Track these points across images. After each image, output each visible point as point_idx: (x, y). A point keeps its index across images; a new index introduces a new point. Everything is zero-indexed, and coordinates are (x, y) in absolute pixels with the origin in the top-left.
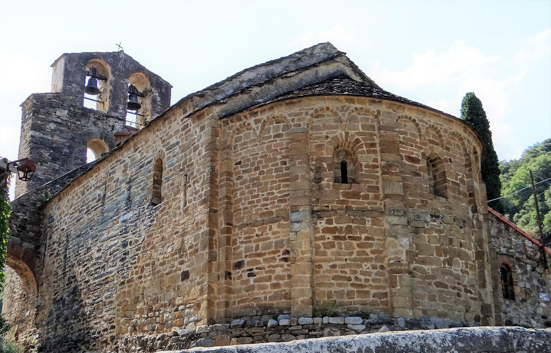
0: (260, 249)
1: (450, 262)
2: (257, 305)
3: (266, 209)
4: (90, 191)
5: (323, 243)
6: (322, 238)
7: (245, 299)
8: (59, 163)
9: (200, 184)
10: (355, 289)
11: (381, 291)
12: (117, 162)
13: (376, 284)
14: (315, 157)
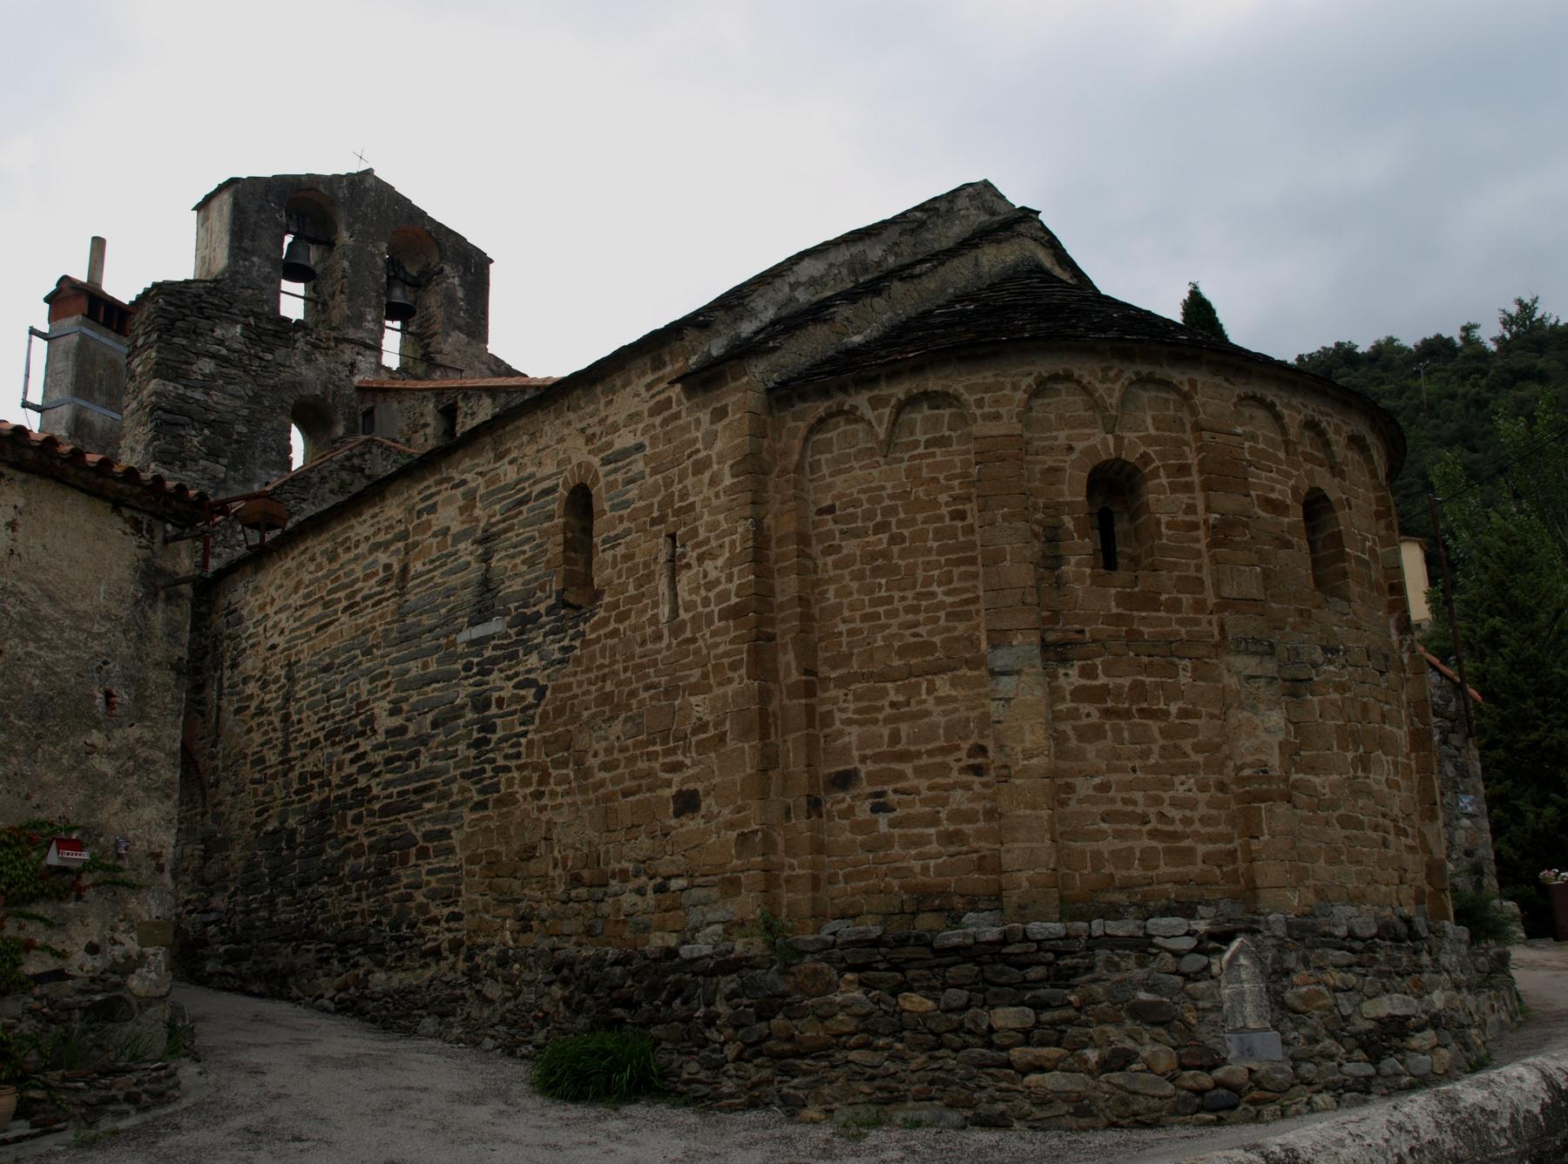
0: (904, 740)
1: (1364, 763)
2: (901, 887)
3: (915, 635)
4: (355, 552)
5: (1074, 728)
6: (1073, 714)
7: (866, 871)
8: (225, 461)
9: (720, 562)
10: (1160, 846)
11: (1221, 846)
12: (440, 482)
13: (1209, 829)
14: (1041, 502)
